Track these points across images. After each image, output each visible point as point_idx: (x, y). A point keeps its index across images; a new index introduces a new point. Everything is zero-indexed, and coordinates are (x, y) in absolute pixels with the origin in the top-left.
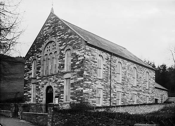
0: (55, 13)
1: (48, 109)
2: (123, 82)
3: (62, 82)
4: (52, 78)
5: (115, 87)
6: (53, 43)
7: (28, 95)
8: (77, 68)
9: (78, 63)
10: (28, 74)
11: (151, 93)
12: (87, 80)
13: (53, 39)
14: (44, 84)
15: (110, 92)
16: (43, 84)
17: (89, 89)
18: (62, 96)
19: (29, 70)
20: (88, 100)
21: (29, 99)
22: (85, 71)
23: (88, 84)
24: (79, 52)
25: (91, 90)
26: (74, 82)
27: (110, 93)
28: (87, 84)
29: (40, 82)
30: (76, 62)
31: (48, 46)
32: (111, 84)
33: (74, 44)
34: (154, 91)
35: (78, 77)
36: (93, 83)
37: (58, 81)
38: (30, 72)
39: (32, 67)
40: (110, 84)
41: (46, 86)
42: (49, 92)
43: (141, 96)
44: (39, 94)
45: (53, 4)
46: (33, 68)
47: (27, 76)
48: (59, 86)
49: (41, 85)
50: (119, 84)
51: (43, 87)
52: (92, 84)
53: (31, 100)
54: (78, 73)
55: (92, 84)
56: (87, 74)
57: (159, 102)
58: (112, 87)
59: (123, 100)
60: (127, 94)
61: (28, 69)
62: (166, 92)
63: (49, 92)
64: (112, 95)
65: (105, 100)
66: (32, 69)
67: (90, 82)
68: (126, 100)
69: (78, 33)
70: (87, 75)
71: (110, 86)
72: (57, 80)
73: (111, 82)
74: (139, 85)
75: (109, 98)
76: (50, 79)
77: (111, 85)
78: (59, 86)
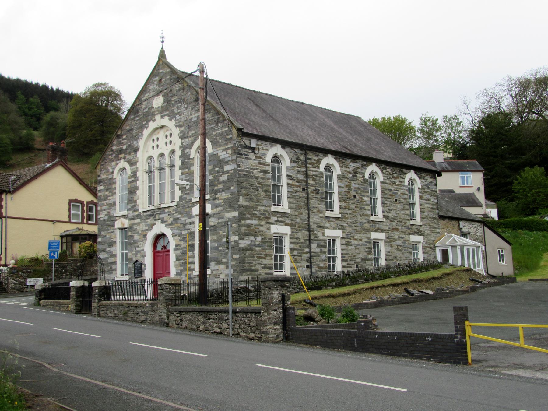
0: (170, 59)
1: (159, 291)
2: (342, 211)
3: (190, 223)
4: (167, 214)
5: (321, 227)
6: (165, 129)
7: (108, 258)
8: (223, 190)
9: (224, 178)
10: (107, 204)
11: (429, 232)
12: (248, 216)
13: (166, 121)
14: (147, 230)
15: (309, 240)
16: (144, 228)
17: (252, 238)
18: (190, 257)
19: (109, 196)
20: (251, 263)
21: (111, 268)
22: (241, 197)
23: (251, 227)
24: (225, 153)
25: (259, 239)
26: (218, 223)
27: (310, 243)
28: (248, 226)
29: (136, 224)
30: (221, 176)
31: (155, 137)
32: (311, 220)
33: (214, 133)
34: (436, 226)
35: (227, 212)
36: (263, 223)
37: (179, 222)
38: (111, 200)
39: (115, 189)
40: (309, 221)
41: (151, 236)
42: (159, 248)
43: (399, 242)
44: (137, 254)
45: (163, 40)
46: (118, 191)
47: (105, 210)
48: (183, 232)
49: (140, 232)
50: (331, 219)
51: (145, 236)
52: (262, 226)
53: (115, 270)
54: (226, 201)
55: (262, 226)
56: (247, 203)
57: (308, 264)
58: (313, 226)
59: (346, 256)
60: (355, 239)
61: (106, 193)
62: (479, 224)
63: (19, 93)
64: (314, 246)
65: (296, 261)
66: (115, 193)
67: (254, 222)
68: (354, 256)
69: (147, 397)
70: (246, 207)
71: (309, 225)
72: (178, 218)
73: (311, 216)
74: (390, 215)
75: (308, 255)
76: (162, 216)
77: (311, 224)
78: (183, 232)
